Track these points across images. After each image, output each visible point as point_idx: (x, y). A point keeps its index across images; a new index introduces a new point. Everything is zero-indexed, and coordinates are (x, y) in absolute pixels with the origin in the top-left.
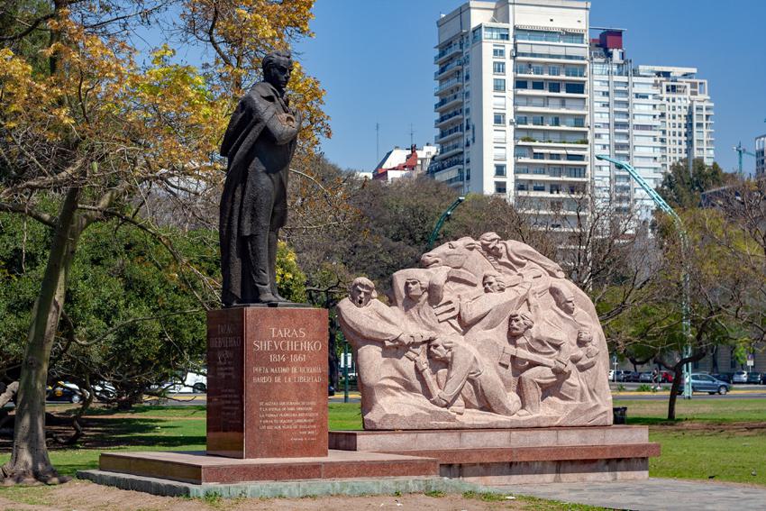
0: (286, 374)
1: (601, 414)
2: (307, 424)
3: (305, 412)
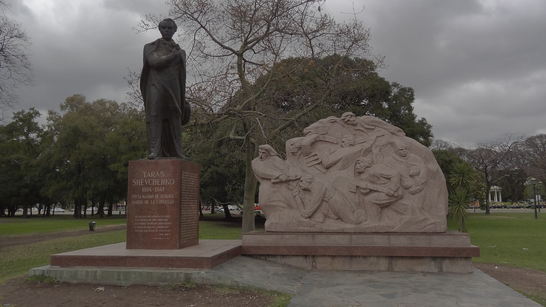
0: (152, 199)
1: (429, 225)
2: (164, 229)
3: (163, 222)
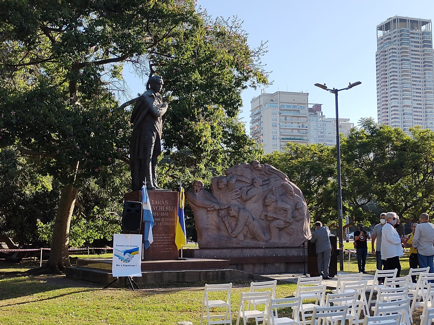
3: (168, 239)
